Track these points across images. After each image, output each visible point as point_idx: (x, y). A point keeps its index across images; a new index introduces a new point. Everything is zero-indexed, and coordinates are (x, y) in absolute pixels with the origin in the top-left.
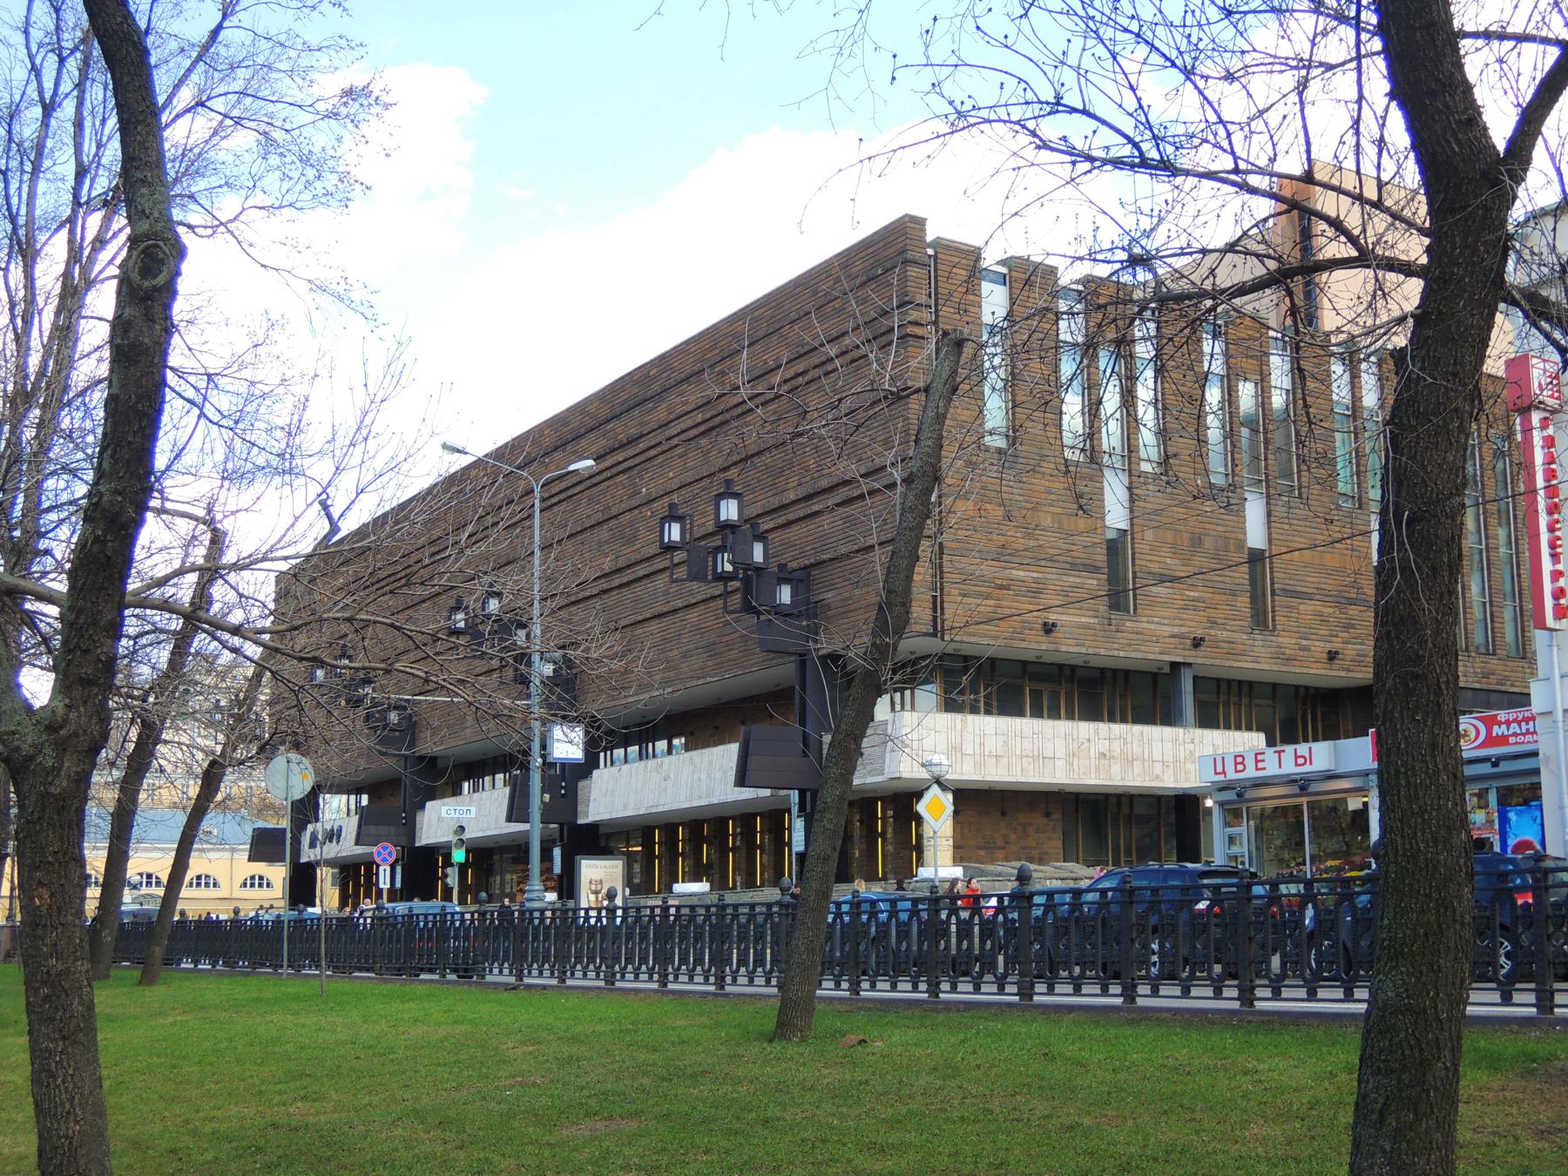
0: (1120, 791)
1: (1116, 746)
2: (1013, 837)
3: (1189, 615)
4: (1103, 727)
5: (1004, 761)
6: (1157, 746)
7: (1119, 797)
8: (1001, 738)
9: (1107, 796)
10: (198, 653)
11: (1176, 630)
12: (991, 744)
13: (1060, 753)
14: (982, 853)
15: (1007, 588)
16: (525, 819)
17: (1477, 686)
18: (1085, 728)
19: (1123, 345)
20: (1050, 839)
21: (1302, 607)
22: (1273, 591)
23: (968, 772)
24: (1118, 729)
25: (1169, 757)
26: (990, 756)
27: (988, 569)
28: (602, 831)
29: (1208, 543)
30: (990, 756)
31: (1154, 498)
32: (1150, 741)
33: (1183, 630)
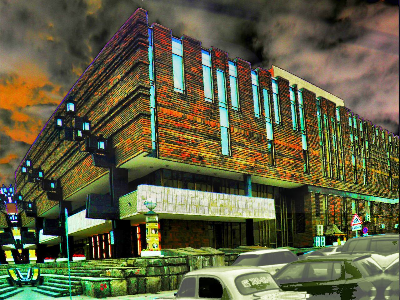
0: (227, 221)
1: (226, 202)
2: (191, 238)
3: (249, 158)
4: (221, 195)
5: (185, 207)
6: (240, 203)
7: (227, 223)
8: (184, 198)
9: (223, 223)
10: (146, 279)
11: (246, 163)
12: (179, 200)
13: (206, 204)
14: (180, 244)
15: (184, 141)
16: (275, 242)
17: (329, 187)
18: (215, 195)
19: (226, 70)
20: (204, 238)
21: (283, 159)
22: (275, 153)
23: (169, 210)
24: (227, 196)
25: (244, 206)
26: (179, 204)
27: (177, 135)
28: (254, 221)
29: (255, 135)
30: (179, 204)
31: (236, 119)
32: (238, 201)
33: (248, 163)
